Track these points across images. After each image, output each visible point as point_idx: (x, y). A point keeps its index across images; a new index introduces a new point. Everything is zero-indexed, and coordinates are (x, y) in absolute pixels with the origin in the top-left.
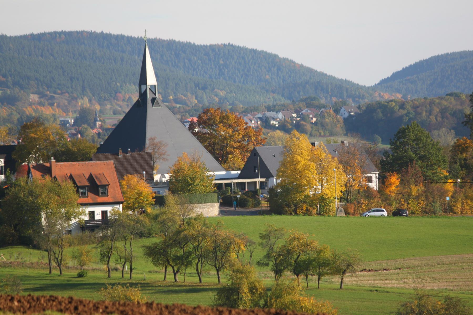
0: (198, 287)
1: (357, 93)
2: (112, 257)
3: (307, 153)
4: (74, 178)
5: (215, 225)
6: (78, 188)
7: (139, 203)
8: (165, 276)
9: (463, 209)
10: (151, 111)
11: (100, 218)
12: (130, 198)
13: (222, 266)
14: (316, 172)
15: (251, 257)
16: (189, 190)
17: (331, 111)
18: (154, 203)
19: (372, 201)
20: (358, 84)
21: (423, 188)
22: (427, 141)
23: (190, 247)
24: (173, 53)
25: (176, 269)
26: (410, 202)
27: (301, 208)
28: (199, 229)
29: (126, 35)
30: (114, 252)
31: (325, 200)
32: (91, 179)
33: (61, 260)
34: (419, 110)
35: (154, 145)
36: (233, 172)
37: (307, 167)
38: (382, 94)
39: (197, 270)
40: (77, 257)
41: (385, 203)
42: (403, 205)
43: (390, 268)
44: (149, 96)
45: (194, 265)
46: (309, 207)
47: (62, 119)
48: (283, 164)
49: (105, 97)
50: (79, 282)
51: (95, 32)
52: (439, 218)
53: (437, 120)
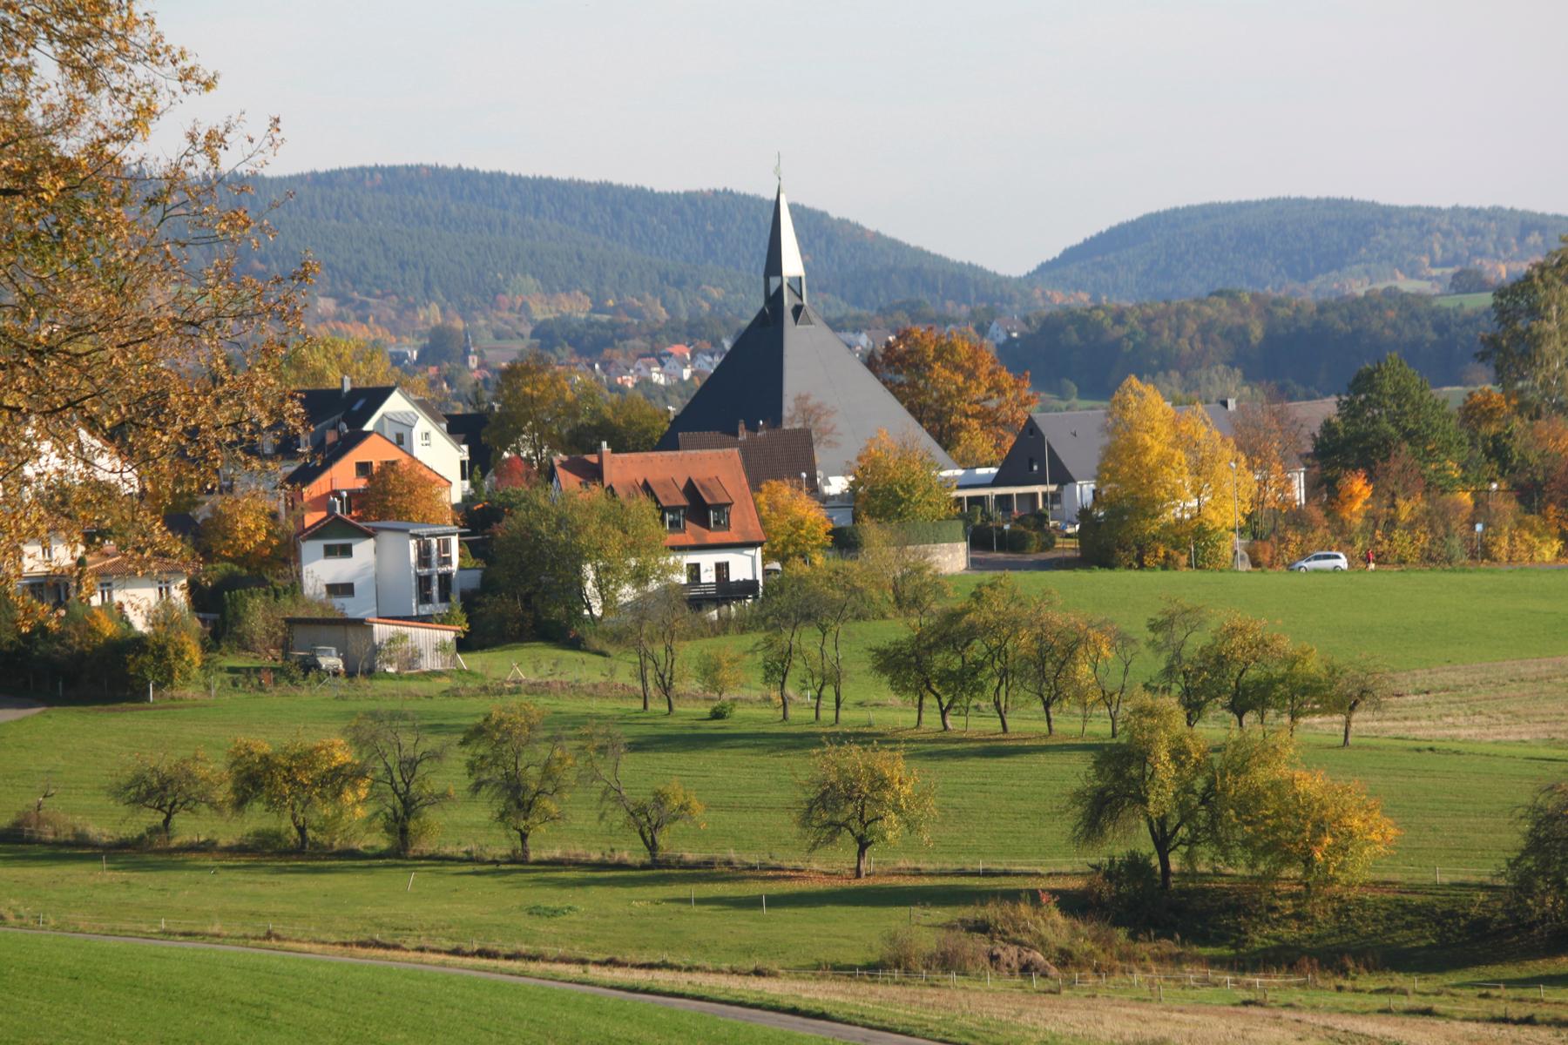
0: (1004, 743)
1: (998, 293)
2: (791, 673)
3: (1166, 429)
4: (654, 489)
5: (1037, 600)
6: (664, 510)
7: (796, 545)
8: (919, 718)
9: (1512, 552)
10: (796, 339)
11: (714, 580)
12: (776, 534)
13: (1058, 693)
14: (1186, 470)
15: (1126, 673)
16: (900, 515)
17: (971, 329)
18: (829, 544)
19: (1310, 535)
20: (995, 274)
21: (1423, 505)
22: (1422, 398)
23: (977, 649)
24: (609, 209)
25: (945, 703)
26: (1396, 536)
27: (1153, 553)
28: (1002, 608)
29: (509, 173)
30: (794, 662)
31: (1208, 533)
32: (691, 490)
33: (671, 679)
34: (1155, 326)
35: (806, 412)
36: (980, 471)
37: (1165, 461)
38: (1049, 293)
39: (997, 704)
40: (710, 672)
41: (1339, 539)
42: (1379, 543)
43: (1404, 690)
44: (788, 301)
45: (990, 692)
46: (1171, 551)
47: (392, 349)
48: (1110, 453)
49: (472, 303)
50: (720, 731)
51: (444, 168)
52: (1470, 572)
53: (1192, 348)
